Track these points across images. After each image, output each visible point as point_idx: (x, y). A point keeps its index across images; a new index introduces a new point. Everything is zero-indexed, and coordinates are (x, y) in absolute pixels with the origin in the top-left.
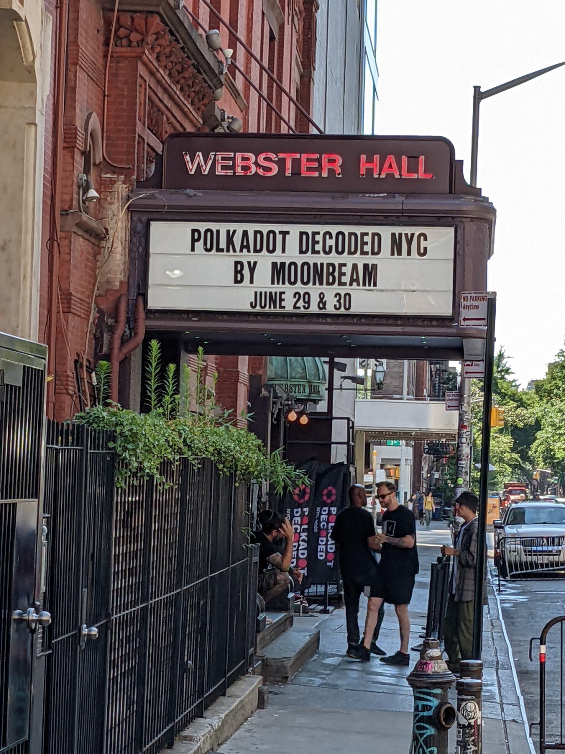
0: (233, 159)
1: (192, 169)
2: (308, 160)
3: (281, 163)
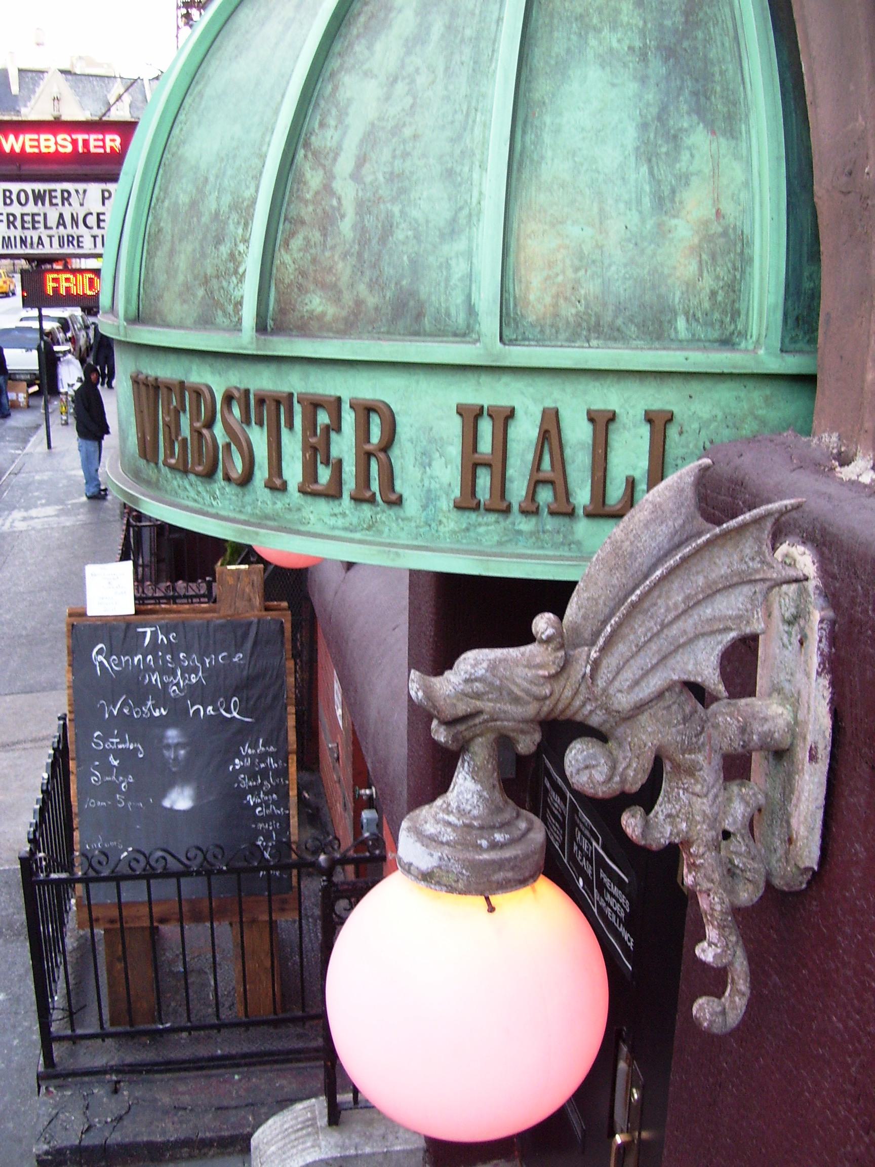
0: (38, 140)
1: (7, 149)
2: (95, 140)
3: (74, 143)
